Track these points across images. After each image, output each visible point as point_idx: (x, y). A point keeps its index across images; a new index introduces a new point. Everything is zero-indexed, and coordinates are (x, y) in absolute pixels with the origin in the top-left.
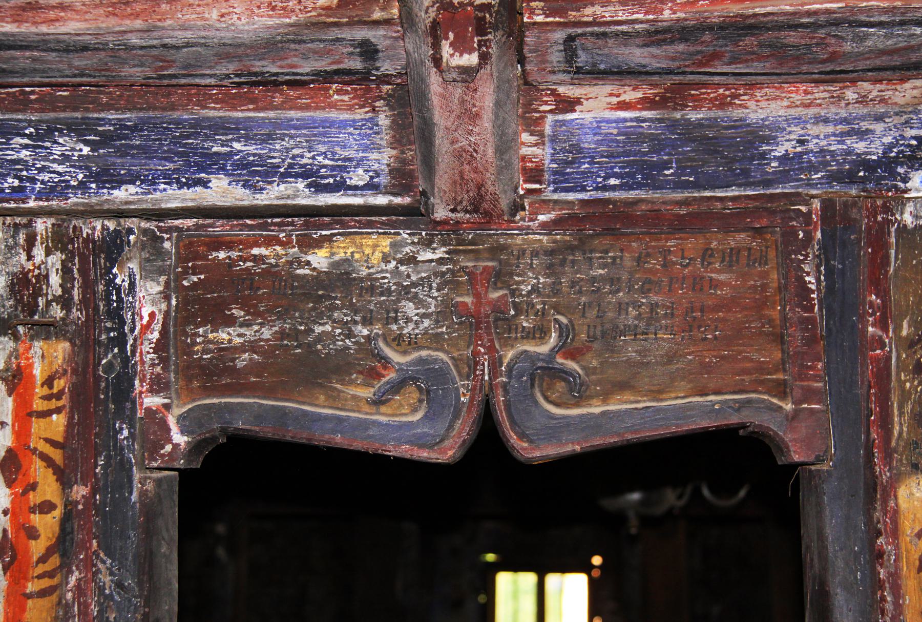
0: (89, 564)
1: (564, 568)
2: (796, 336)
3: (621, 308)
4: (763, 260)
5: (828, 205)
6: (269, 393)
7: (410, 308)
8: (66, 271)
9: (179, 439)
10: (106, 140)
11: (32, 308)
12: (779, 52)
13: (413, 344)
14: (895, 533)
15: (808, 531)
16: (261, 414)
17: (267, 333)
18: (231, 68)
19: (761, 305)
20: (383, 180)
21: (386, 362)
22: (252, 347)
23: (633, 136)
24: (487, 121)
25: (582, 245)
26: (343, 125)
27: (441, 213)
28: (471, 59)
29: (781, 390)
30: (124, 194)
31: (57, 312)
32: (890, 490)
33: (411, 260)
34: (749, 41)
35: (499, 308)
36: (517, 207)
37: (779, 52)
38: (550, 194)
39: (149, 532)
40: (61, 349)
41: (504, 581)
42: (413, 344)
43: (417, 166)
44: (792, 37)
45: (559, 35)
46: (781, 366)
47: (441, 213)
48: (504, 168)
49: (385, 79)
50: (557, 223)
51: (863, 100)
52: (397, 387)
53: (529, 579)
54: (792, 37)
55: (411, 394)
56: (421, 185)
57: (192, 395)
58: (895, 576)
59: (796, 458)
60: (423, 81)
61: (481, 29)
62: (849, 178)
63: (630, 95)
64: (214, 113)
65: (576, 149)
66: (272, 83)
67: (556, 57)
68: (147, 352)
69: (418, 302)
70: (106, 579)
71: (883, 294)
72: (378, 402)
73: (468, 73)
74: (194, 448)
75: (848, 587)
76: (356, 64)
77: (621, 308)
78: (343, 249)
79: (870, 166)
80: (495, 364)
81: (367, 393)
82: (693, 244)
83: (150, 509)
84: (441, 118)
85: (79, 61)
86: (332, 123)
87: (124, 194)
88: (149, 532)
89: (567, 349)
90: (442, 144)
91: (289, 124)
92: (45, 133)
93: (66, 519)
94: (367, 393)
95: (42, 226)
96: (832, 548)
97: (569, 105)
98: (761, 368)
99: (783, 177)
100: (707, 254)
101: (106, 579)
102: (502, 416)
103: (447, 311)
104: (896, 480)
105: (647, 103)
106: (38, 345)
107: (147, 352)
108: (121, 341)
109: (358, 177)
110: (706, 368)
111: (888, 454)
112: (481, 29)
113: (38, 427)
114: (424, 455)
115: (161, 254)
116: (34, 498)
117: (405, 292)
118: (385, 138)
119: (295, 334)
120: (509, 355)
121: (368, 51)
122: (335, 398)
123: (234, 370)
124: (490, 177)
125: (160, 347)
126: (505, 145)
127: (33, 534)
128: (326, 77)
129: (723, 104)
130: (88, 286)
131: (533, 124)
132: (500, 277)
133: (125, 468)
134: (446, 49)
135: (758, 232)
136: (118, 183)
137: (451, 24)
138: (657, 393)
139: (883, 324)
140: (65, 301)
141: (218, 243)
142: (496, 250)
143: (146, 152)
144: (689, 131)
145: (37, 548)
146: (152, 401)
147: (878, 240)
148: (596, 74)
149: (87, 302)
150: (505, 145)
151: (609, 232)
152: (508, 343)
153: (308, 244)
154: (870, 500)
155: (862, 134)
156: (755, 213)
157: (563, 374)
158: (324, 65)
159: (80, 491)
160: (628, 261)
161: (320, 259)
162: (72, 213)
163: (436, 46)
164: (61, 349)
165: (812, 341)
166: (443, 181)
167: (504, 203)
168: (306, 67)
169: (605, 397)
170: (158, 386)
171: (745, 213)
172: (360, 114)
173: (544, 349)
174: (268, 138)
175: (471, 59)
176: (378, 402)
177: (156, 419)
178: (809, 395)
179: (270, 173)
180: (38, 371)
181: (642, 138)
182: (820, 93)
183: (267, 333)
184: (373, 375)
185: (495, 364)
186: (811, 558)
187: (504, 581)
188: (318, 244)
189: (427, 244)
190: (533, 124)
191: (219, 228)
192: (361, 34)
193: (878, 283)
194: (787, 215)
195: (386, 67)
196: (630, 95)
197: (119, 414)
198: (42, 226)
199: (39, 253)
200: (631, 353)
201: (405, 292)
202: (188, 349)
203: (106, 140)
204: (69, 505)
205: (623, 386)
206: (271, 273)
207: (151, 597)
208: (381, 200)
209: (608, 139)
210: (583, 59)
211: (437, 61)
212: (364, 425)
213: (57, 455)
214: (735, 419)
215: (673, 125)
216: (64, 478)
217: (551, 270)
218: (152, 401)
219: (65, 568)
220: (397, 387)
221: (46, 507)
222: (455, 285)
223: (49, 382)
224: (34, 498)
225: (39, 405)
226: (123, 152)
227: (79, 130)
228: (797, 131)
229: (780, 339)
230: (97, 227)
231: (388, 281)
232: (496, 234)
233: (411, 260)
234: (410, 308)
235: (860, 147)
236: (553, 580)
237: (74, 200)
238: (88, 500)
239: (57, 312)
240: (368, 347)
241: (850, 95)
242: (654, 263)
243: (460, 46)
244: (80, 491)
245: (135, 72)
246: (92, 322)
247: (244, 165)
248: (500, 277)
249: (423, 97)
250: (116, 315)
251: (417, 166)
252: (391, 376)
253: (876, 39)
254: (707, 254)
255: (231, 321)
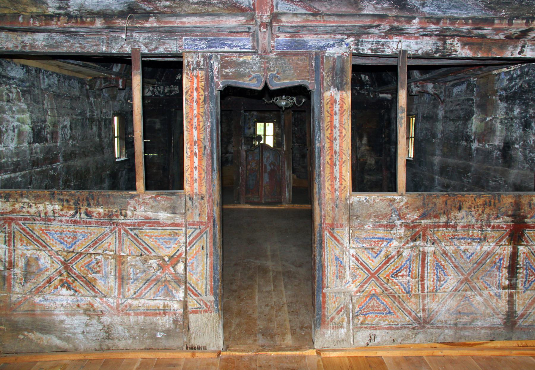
0: (208, 103)
1: (269, 122)
2: (311, 71)
3: (286, 67)
4: (306, 60)
5: (316, 53)
6: (234, 79)
7: (254, 67)
8: (204, 61)
9: (221, 86)
10: (209, 41)
11: (199, 66)
12: (309, 30)
13: (255, 72)
14: (324, 100)
15: (312, 100)
16: (233, 82)
17: (233, 70)
18: (229, 30)
19: (306, 67)
20: (251, 48)
21: (251, 75)
22: (231, 72)
23: (288, 42)
24: (267, 39)
25: (280, 58)
26: (244, 39)
27: (259, 53)
28: (265, 30)
29: (309, 79)
30: (212, 49)
31: (202, 67)
32: (323, 94)
33: (255, 60)
34: (305, 28)
35: (268, 67)
36: (271, 52)
37: (309, 30)
38: (275, 50)
39: (217, 99)
40: (203, 72)
41: (258, 124)
42: (255, 72)
43: (256, 46)
44: (311, 28)
45: (278, 27)
46: (309, 76)
47: (259, 53)
48: (269, 46)
49: (251, 32)
50: (277, 54)
51: (321, 37)
52: (253, 78)
53: (262, 124)
54: (311, 28)
55: (255, 80)
56: (256, 48)
57: (222, 79)
58: (323, 106)
59: (310, 89)
60: (257, 33)
61: (267, 26)
62: (319, 49)
63: (287, 36)
64: (225, 37)
65: (279, 43)
66: (234, 33)
67: (277, 30)
68: (216, 73)
69: (256, 66)
70: (211, 106)
71: (323, 66)
72: (250, 81)
73: (265, 32)
74: (223, 87)
75: (317, 107)
76: (247, 30)
77: (286, 67)
78: (245, 58)
79: (322, 47)
80: (267, 75)
81: (248, 79)
82: (296, 58)
83: (217, 96)
84: (260, 39)
85: (207, 29)
86: (243, 39)
87: (212, 49)
88: (217, 99)
89: (277, 73)
90: (260, 42)
91: (236, 39)
92: (201, 40)
93: (205, 97)
94: (248, 79)
95: (200, 54)
96: (315, 102)
97: (278, 37)
98: (306, 76)
99: (309, 48)
100: (298, 59)
101: (211, 106)
102: (268, 83)
103: (260, 67)
104: (324, 92)
105: (290, 37)
106: (200, 72)
107: (216, 73)
108: (212, 71)
109: (247, 47)
110: (298, 76)
111: (323, 89)
112: (267, 26)
113: (200, 84)
114: (257, 88)
115: (217, 58)
116: (200, 94)
117: (254, 64)
118: (251, 41)
119: (237, 70)
120: (269, 74)
121: (249, 28)
122: (243, 80)
123: (228, 76)
124: (267, 47)
125: (218, 72)
126: (269, 43)
127: (200, 99)
128: (242, 32)
129: (301, 37)
130: (207, 63)
131: (273, 40)
132: (268, 62)
133: (213, 90)
134: (262, 28)
135: (306, 56)
136: (211, 47)
137: (262, 25)
138: (291, 80)
139: (323, 70)
140: (204, 65)
141: (226, 57)
142: (267, 58)
143: (215, 43)
144: (296, 41)
145: (201, 101)
146: (217, 80)
147: (323, 58)
148: (283, 32)
149: (207, 65)
150: (269, 43)
151: (284, 56)
152: (269, 72)
153: (239, 57)
154: (320, 95)
155: (321, 42)
156: (305, 54)
157: (277, 77)
158: (243, 30)
159: (207, 93)
160: (287, 60)
161: (241, 59)
162: (204, 52)
163: (260, 28)
164: (203, 72)
165: (313, 72)
166: (260, 48)
167: (269, 51)
168: (239, 31)
169: (283, 80)
170: (218, 78)
171: (303, 54)
172: (247, 38)
173: (274, 73)
174: (233, 41)
175: (265, 30)
176: (250, 81)
177: (217, 83)
178: (312, 80)
179: (234, 46)
180: (200, 76)
181: (289, 42)
182: (315, 36)
183: (233, 70)
184: (249, 77)
185: (267, 75)
186: (312, 103)
187: (258, 124)
188: (241, 57)
189: (257, 57)
190: (273, 40)
191: (226, 54)
192: (248, 26)
193: (322, 64)
194: (310, 54)
195: (251, 31)
196: (287, 36)
197: (212, 82)
198: (200, 54)
199: (200, 58)
200: (287, 74)
201: (254, 64)
202: (222, 73)
203: (209, 41)
204: (205, 95)
205: (286, 79)
206: (234, 61)
207: (217, 109)
208: (250, 51)
209: (284, 42)
210: (281, 30)
211: (260, 30)
212: (248, 84)
213: (203, 88)
214: (302, 84)
215: (294, 40)
216: (204, 91)
217: (276, 61)
218: (217, 80)
219: (205, 104)
220: (253, 78)
221: (202, 95)
222: (261, 63)
223: (202, 77)
224: (200, 94)
225: (200, 80)
226: (212, 43)
227: (205, 40)
228: (311, 42)
229: (309, 72)
230: (208, 54)
231: (251, 63)
232: (267, 56)
233: (255, 60)
234: (254, 67)
235: (320, 44)
236: (267, 124)
237: (205, 50)
238: (208, 94)
239: (202, 67)
240: (248, 73)
241: (319, 36)
242: (291, 61)
243: (264, 28)
244: (207, 93)
245: (214, 31)
246: (208, 68)
247: (230, 45)
248: (268, 62)
249: (257, 35)
250: (211, 67)
251: (256, 46)
252: (252, 77)
253: (322, 29)
254: (298, 59)
255: (228, 68)
